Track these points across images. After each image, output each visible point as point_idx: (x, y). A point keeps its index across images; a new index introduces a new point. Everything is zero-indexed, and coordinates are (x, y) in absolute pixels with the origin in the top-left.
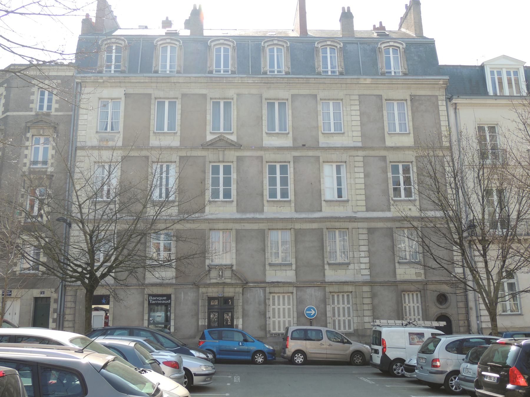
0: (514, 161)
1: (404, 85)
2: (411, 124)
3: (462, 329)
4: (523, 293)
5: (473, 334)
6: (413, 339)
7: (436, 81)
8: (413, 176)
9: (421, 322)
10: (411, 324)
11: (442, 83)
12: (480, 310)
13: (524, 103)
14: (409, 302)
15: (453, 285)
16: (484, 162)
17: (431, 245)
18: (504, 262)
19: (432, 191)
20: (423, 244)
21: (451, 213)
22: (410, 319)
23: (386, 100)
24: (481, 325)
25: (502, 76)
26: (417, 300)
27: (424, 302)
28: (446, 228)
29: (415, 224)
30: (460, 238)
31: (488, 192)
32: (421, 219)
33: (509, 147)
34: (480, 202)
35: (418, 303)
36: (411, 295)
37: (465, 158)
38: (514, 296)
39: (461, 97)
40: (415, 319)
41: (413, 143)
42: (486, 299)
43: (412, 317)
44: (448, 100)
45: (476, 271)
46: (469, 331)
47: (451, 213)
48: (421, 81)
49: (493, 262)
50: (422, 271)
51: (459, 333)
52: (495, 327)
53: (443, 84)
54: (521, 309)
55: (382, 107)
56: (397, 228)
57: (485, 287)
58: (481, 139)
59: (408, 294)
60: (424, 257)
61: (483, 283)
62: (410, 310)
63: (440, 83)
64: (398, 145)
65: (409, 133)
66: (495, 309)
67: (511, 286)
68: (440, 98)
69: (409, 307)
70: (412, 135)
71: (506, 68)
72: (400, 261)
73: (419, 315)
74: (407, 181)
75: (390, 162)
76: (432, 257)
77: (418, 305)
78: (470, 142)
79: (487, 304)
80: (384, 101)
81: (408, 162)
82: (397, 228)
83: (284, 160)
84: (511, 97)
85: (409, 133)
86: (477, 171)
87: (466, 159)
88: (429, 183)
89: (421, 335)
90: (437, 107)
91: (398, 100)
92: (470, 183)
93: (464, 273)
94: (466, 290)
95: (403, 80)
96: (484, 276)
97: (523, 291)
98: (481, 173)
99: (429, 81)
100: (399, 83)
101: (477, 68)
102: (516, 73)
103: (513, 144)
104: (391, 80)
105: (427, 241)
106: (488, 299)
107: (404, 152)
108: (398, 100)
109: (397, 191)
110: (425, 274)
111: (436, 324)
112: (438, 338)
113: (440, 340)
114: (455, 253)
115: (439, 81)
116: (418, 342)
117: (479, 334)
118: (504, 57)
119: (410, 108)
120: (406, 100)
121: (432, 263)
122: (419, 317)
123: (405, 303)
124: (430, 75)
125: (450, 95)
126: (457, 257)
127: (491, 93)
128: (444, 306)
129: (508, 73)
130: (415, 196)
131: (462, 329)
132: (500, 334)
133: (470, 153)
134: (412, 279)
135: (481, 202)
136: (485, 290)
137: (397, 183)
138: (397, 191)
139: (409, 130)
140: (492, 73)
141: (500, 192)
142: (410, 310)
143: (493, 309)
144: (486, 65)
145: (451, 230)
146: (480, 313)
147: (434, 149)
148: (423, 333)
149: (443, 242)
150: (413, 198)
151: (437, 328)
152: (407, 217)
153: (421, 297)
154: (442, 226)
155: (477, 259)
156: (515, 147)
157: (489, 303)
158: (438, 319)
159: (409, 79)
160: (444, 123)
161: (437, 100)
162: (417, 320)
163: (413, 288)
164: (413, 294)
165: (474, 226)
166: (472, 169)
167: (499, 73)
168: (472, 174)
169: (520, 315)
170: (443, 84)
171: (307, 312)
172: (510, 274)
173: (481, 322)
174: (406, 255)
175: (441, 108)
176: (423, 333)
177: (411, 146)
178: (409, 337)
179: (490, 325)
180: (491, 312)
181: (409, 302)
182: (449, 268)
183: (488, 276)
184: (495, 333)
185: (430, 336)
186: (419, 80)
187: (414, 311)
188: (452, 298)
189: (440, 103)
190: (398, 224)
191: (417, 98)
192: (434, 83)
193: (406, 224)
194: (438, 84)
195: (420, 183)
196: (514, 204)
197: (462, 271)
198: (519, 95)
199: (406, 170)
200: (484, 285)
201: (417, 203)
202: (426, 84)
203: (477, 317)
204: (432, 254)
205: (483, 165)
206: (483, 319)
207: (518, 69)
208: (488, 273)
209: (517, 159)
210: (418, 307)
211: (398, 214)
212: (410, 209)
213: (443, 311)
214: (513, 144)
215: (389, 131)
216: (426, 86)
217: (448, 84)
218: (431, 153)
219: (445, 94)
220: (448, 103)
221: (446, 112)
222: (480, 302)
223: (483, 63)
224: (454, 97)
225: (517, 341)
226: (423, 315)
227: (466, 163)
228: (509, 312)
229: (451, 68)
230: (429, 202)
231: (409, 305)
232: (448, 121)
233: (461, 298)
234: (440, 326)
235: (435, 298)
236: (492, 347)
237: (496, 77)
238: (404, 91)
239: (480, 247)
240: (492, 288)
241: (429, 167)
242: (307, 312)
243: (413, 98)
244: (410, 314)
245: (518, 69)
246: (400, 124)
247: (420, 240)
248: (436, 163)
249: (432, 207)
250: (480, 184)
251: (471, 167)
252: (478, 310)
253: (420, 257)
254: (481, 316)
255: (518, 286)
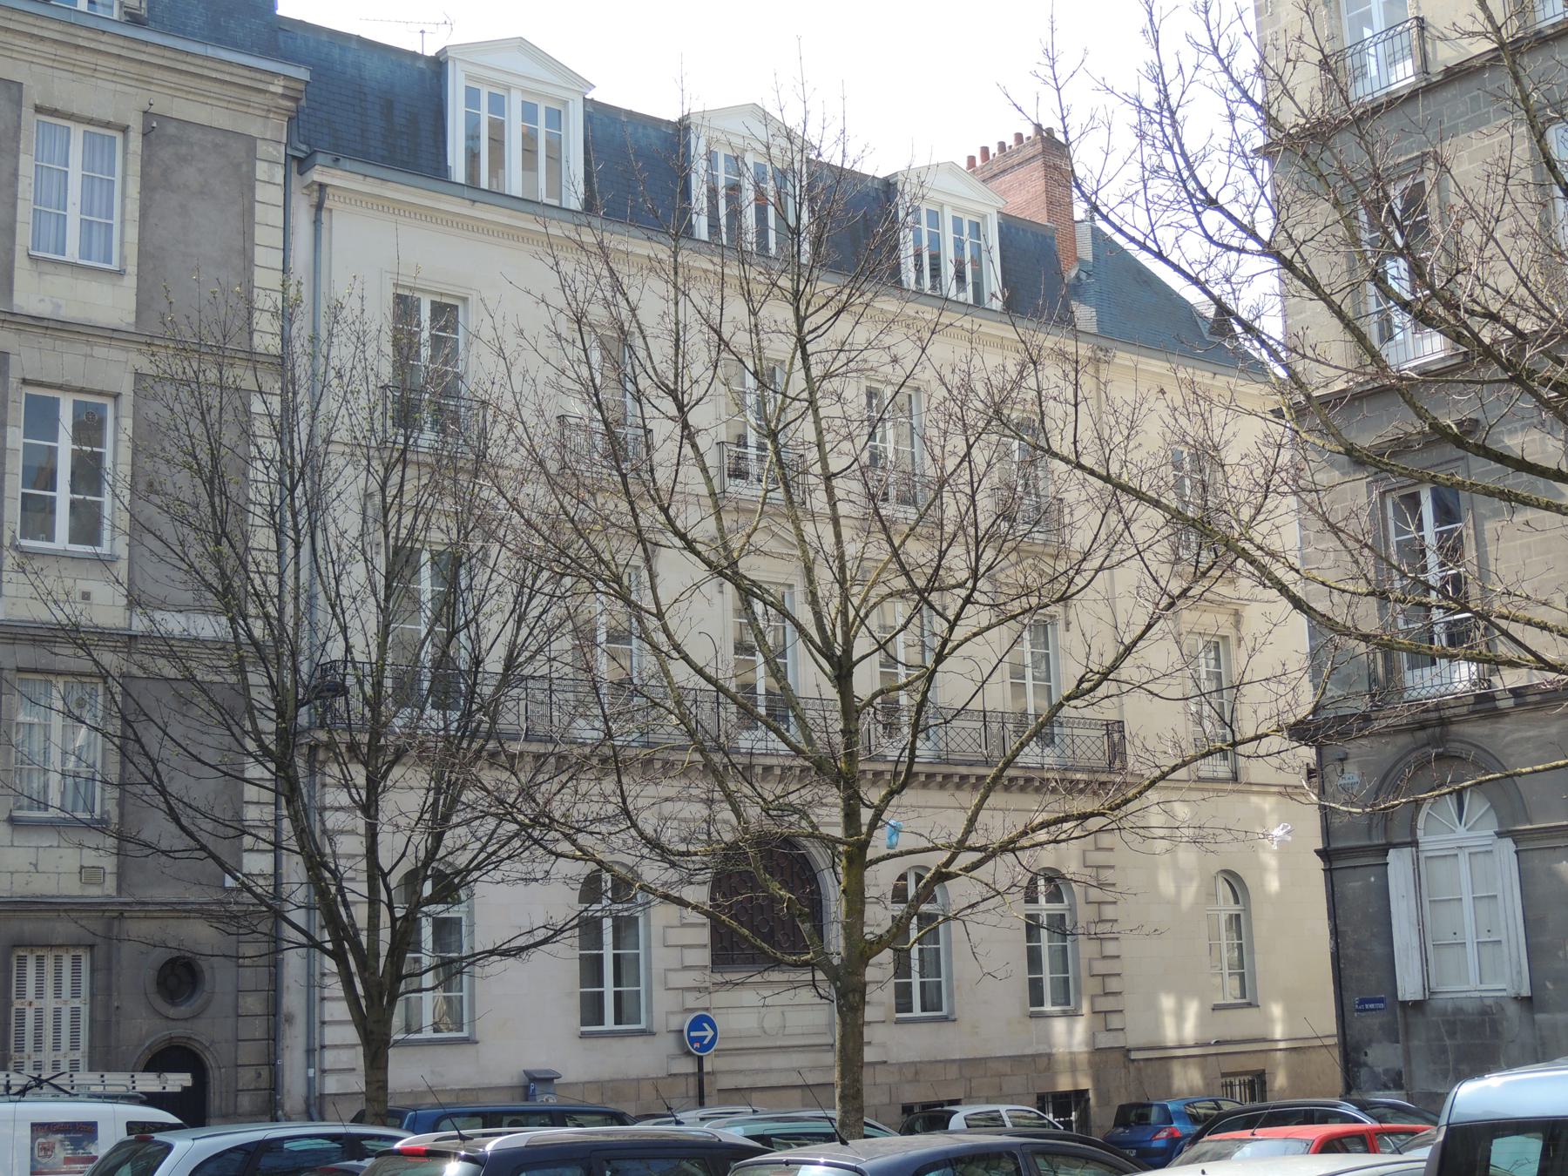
0: (523, 451)
1: (121, 65)
2: (132, 234)
3: (245, 1102)
4: (497, 958)
5: (289, 1119)
6: (47, 1150)
7: (258, 76)
8: (116, 454)
9: (85, 1077)
10: (45, 1086)
11: (280, 90)
12: (323, 1023)
13: (584, 238)
14: (40, 994)
15: (222, 916)
16: (411, 441)
17: (169, 753)
18: (438, 839)
19: (197, 529)
20: (128, 744)
21: (258, 628)
22: (38, 1066)
23: (39, 109)
24: (322, 1084)
25: (506, 119)
26: (76, 984)
27: (103, 993)
28: (232, 686)
29: (108, 659)
30: (281, 735)
31: (402, 562)
32: (129, 641)
33: (508, 395)
34: (375, 595)
35: (75, 994)
36: (49, 964)
37: (343, 410)
38: (450, 970)
39: (347, 164)
40: (56, 1065)
41: (132, 318)
42: (357, 981)
43: (47, 1056)
44: (294, 166)
45: (330, 871)
46: (271, 1110)
47: (258, 628)
48: (199, 62)
49: (401, 839)
50: (109, 864)
51: (233, 1116)
52: (379, 1088)
53: (283, 96)
54: (472, 1021)
55: (16, 138)
56: (19, 670)
57: (357, 934)
58: (404, 348)
59: (40, 959)
60: (121, 803)
61: (350, 916)
62: (39, 1027)
63: (272, 88)
64: (69, 313)
65: (121, 273)
66: (387, 1022)
67: (445, 929)
68: (262, 149)
69: (39, 1011)
70: (131, 281)
71: (524, 91)
72: (16, 813)
73: (74, 1046)
74: (88, 472)
75: (25, 382)
76: (163, 806)
77: (76, 1003)
78: (371, 352)
79: (357, 998)
80: (27, 113)
81: (100, 393)
82: (19, 670)
83: (60, 381)
84: (526, 203)
85: (121, 273)
86: (382, 472)
87: (346, 420)
88: (187, 495)
89: (87, 1130)
90: (248, 184)
91: (90, 121)
92: (345, 518)
93: (276, 874)
94: (276, 945)
95: (121, 42)
96: (358, 887)
97: (492, 953)
98: (395, 479)
99: (231, 69)
100: (102, 47)
101: (421, 64)
102: (555, 118)
103: (527, 389)
104: (72, 30)
105: (151, 737)
106: (364, 982)
107: (87, 350)
108: (90, 121)
109: (38, 513)
110: (121, 875)
111: (149, 1083)
112: (162, 1143)
113: (168, 1148)
114: (251, 792)
115: (268, 78)
116: (67, 1161)
117: (311, 1119)
118: (522, 45)
119: (135, 167)
120: (125, 130)
121: (158, 829)
122: (77, 1055)
123: (21, 994)
124: (235, 46)
125: (304, 147)
126: (258, 806)
127: (459, 172)
128: (183, 1010)
129: (529, 112)
130: (114, 543)
131: (245, 1102)
132: (393, 1117)
133: (363, 394)
134: (66, 893)
135: (382, 595)
136: (356, 945)
137: (42, 475)
138: (38, 513)
139: (123, 258)
140: (472, 96)
141: (451, 566)
142: (39, 1027)
143: (379, 1021)
144: (454, 60)
145: (251, 699)
146: (322, 1034)
147: (221, 357)
148: (94, 1124)
149: (212, 744)
150: (104, 549)
151: (152, 1100)
152: (76, 628)
153: (93, 971)
154: (217, 679)
155: (333, 820)
156: (531, 398)
157: (368, 996)
158: (159, 1062)
159: (146, 43)
160: (267, 256)
161: (252, 156)
162: (65, 1067)
163: (63, 929)
164: (58, 958)
165: (341, 690)
166: (365, 462)
167: (497, 103)
168: (361, 482)
169: (642, 1033)
170: (283, 96)
171: (693, 1034)
172: (450, 887)
173: (323, 1071)
174: (46, 787)
175: (262, 193)
176: (94, 1124)
177: (123, 327)
178: (33, 1140)
179: (357, 1083)
180: (372, 1032)
181: (40, 994)
182: (222, 849)
183: (373, 889)
184: (376, 1115)
185: (122, 1135)
186: (189, 59)
187: (57, 1029)
188: (219, 977)
189: (262, 170)
190: (26, 655)
191: (171, 129)
192: (248, 83)
193: (67, 658)
194: (265, 92)
195: (144, 487)
196: (499, 617)
197: (269, 869)
198: (555, 202)
199: (89, 426)
200: (353, 925)
201: (122, 569)
202: (216, 80)
203: (310, 1052)
204: (163, 792)
205: (404, 452)
206: (330, 1059)
207: (565, 103)
208: (375, 874)
209: (532, 445)
210: (75, 1012)
211: (40, 613)
212: (86, 596)
213: (179, 1030)
214: (527, 389)
215: (36, 246)
216: (216, 88)
217: (303, 103)
218: (212, 375)
219: (284, 141)
220: (295, 176)
221: (281, 211)
222: (327, 993)
223: (444, 51)
224: (320, 158)
225: (468, 1143)
226: (92, 1047)
227: (342, 435)
228: (428, 1034)
229: (324, 38)
230: (180, 576)
231: (37, 1004)
232: (286, 250)
233: (253, 976)
234: (168, 1089)
235: (149, 975)
236: (373, 1169)
237: (485, 116)
238: (119, 87)
239: (359, 774)
240: (385, 935)
241: (198, 430)
242: (693, 1034)
243: (154, 128)
244: (38, 1041)
245: (565, 103)
246: (87, 226)
247: (115, 726)
248: (225, 417)
249: (188, 597)
250: (385, 526)
251: (358, 452)
252: (315, 1023)
253: (105, 802)
254: (323, 1047)
255: (472, 933)
